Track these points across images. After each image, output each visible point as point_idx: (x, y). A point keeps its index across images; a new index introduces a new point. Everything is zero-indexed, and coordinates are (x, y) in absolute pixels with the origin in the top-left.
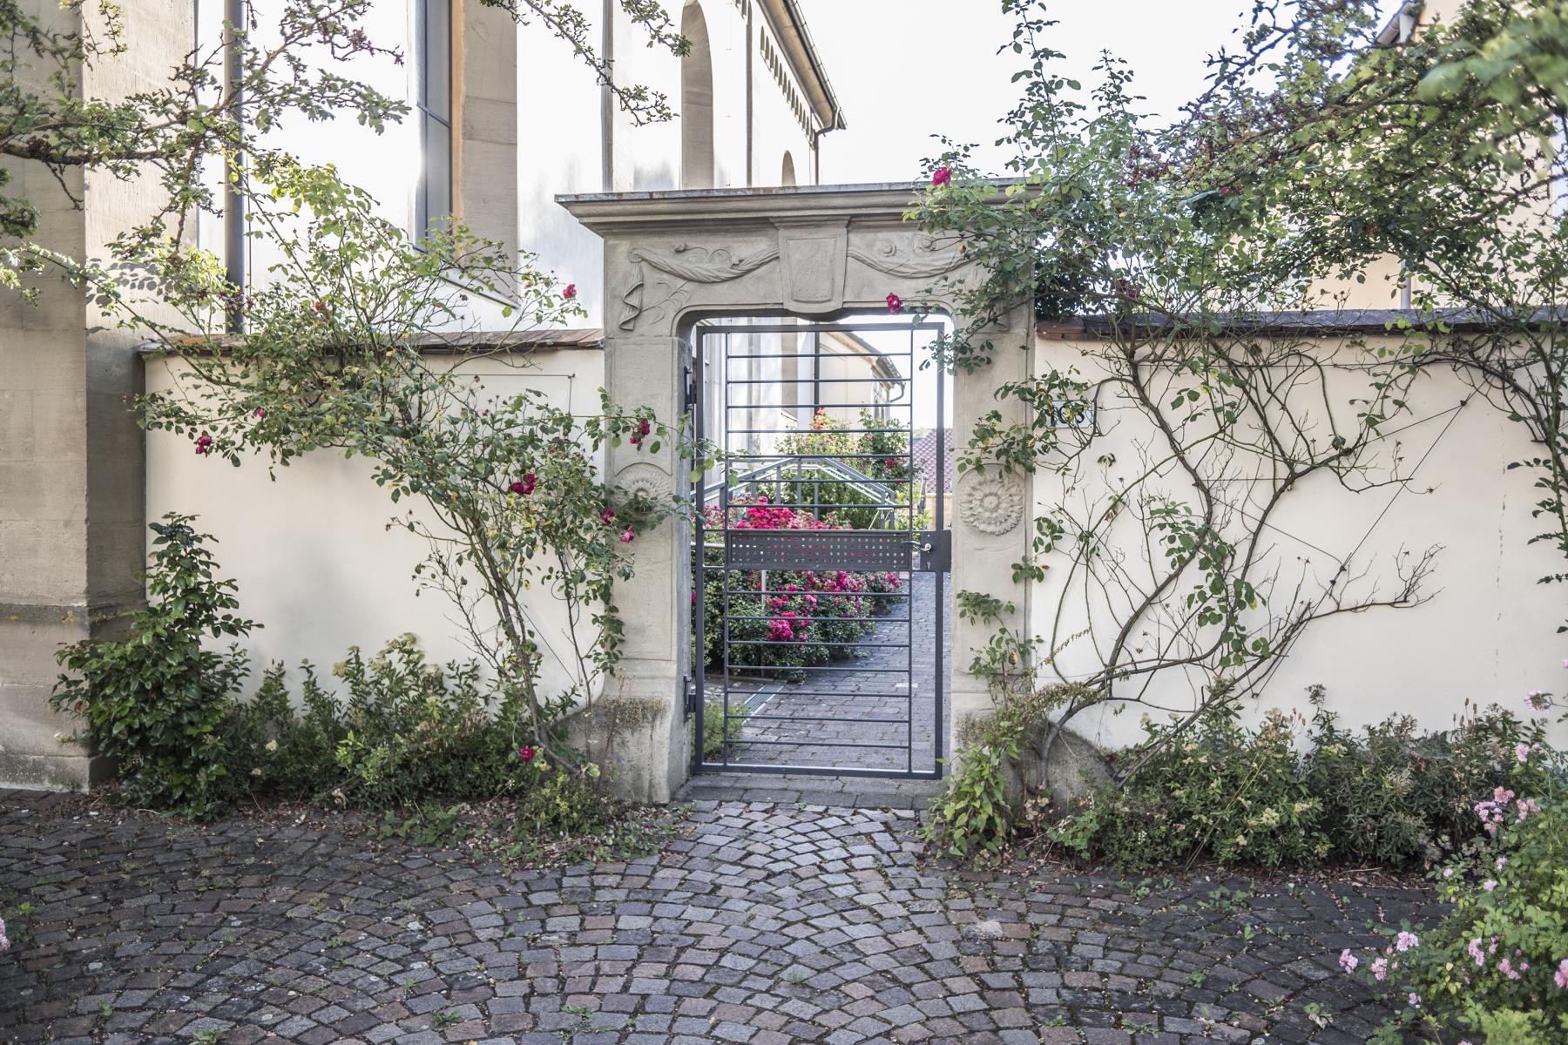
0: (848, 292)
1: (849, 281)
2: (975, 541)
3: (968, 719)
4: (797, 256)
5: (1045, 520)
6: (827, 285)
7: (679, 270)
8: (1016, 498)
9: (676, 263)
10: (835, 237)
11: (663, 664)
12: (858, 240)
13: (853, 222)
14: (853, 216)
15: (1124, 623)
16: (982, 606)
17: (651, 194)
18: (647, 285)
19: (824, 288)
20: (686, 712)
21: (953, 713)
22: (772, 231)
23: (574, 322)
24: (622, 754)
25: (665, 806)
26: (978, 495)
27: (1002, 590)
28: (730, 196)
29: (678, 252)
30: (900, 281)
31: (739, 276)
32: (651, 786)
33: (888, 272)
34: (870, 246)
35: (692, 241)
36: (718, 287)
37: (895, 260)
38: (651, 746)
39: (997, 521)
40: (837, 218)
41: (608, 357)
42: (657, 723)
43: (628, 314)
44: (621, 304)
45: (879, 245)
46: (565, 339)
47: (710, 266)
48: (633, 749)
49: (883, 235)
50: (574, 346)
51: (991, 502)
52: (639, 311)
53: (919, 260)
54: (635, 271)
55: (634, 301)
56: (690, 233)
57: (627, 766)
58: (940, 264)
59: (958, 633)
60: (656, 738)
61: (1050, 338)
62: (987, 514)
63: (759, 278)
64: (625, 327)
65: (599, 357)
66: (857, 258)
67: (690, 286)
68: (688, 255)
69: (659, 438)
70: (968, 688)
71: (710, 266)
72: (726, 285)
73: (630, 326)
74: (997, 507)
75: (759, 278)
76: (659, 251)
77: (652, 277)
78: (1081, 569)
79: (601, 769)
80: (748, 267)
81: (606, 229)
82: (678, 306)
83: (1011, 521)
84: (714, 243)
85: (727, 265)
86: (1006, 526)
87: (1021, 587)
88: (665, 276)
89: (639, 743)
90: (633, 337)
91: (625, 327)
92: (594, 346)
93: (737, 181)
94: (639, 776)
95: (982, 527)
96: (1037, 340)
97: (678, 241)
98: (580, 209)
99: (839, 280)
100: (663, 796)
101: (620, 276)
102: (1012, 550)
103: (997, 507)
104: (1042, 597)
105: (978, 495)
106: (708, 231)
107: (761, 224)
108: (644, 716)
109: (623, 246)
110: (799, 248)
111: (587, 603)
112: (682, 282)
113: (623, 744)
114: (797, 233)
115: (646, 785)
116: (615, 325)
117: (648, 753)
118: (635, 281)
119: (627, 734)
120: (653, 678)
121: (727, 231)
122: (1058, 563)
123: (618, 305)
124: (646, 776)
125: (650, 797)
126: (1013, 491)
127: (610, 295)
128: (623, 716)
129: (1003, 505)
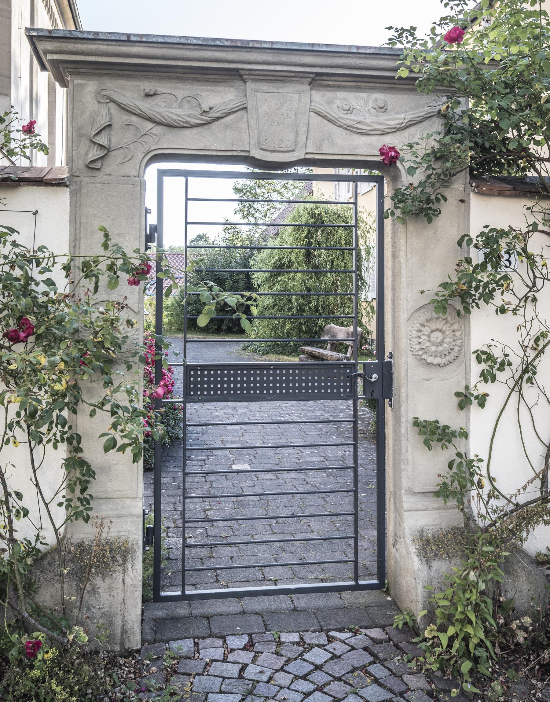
0: (310, 144)
1: (311, 134)
2: (421, 372)
3: (421, 536)
4: (264, 108)
5: (484, 353)
6: (291, 136)
7: (149, 112)
8: (458, 334)
9: (145, 106)
10: (299, 92)
11: (128, 502)
12: (320, 98)
13: (318, 80)
14: (318, 74)
16: (435, 434)
17: (129, 36)
18: (116, 126)
19: (288, 140)
21: (407, 531)
23: (40, 160)
24: (93, 602)
25: (138, 651)
26: (426, 330)
27: (448, 417)
29: (147, 95)
30: (356, 137)
32: (124, 631)
33: (347, 128)
34: (330, 102)
35: (161, 87)
36: (187, 132)
37: (352, 117)
38: (124, 591)
39: (443, 354)
41: (73, 195)
42: (129, 565)
43: (95, 153)
44: (88, 142)
45: (338, 102)
47: (179, 111)
48: (104, 595)
49: (341, 94)
50: (39, 182)
51: (437, 336)
52: (107, 150)
53: (374, 119)
54: (104, 112)
55: (103, 140)
56: (159, 78)
57: (98, 615)
58: (393, 123)
59: (410, 456)
60: (128, 581)
61: (481, 193)
62: (434, 348)
63: (227, 126)
64: (92, 167)
65: (63, 197)
66: (318, 114)
67: (158, 130)
69: (160, 275)
70: (419, 506)
71: (179, 111)
72: (194, 131)
73: (97, 165)
74: (442, 342)
75: (227, 126)
76: (128, 93)
77: (120, 118)
78: (515, 395)
79: (86, 632)
83: (454, 354)
84: (183, 90)
85: (197, 112)
87: (462, 413)
88: (134, 118)
89: (111, 589)
90: (100, 177)
91: (92, 167)
92: (59, 183)
94: (111, 623)
95: (429, 360)
96: (472, 195)
97: (149, 86)
99: (302, 133)
100: (135, 641)
101: (87, 115)
102: (451, 381)
103: (442, 342)
104: (479, 421)
105: (426, 330)
106: (177, 78)
107: (232, 75)
108: (114, 558)
109: (90, 86)
110: (266, 100)
111: (55, 447)
112: (150, 125)
113: (94, 591)
114: (264, 86)
115: (119, 631)
116: (80, 164)
117: (120, 598)
118: (103, 121)
119: (98, 581)
120: (119, 517)
121: (195, 80)
122: (497, 392)
123: (85, 144)
124: (118, 622)
125: (122, 644)
126: (456, 326)
127: (76, 134)
128: (88, 562)
129: (447, 340)
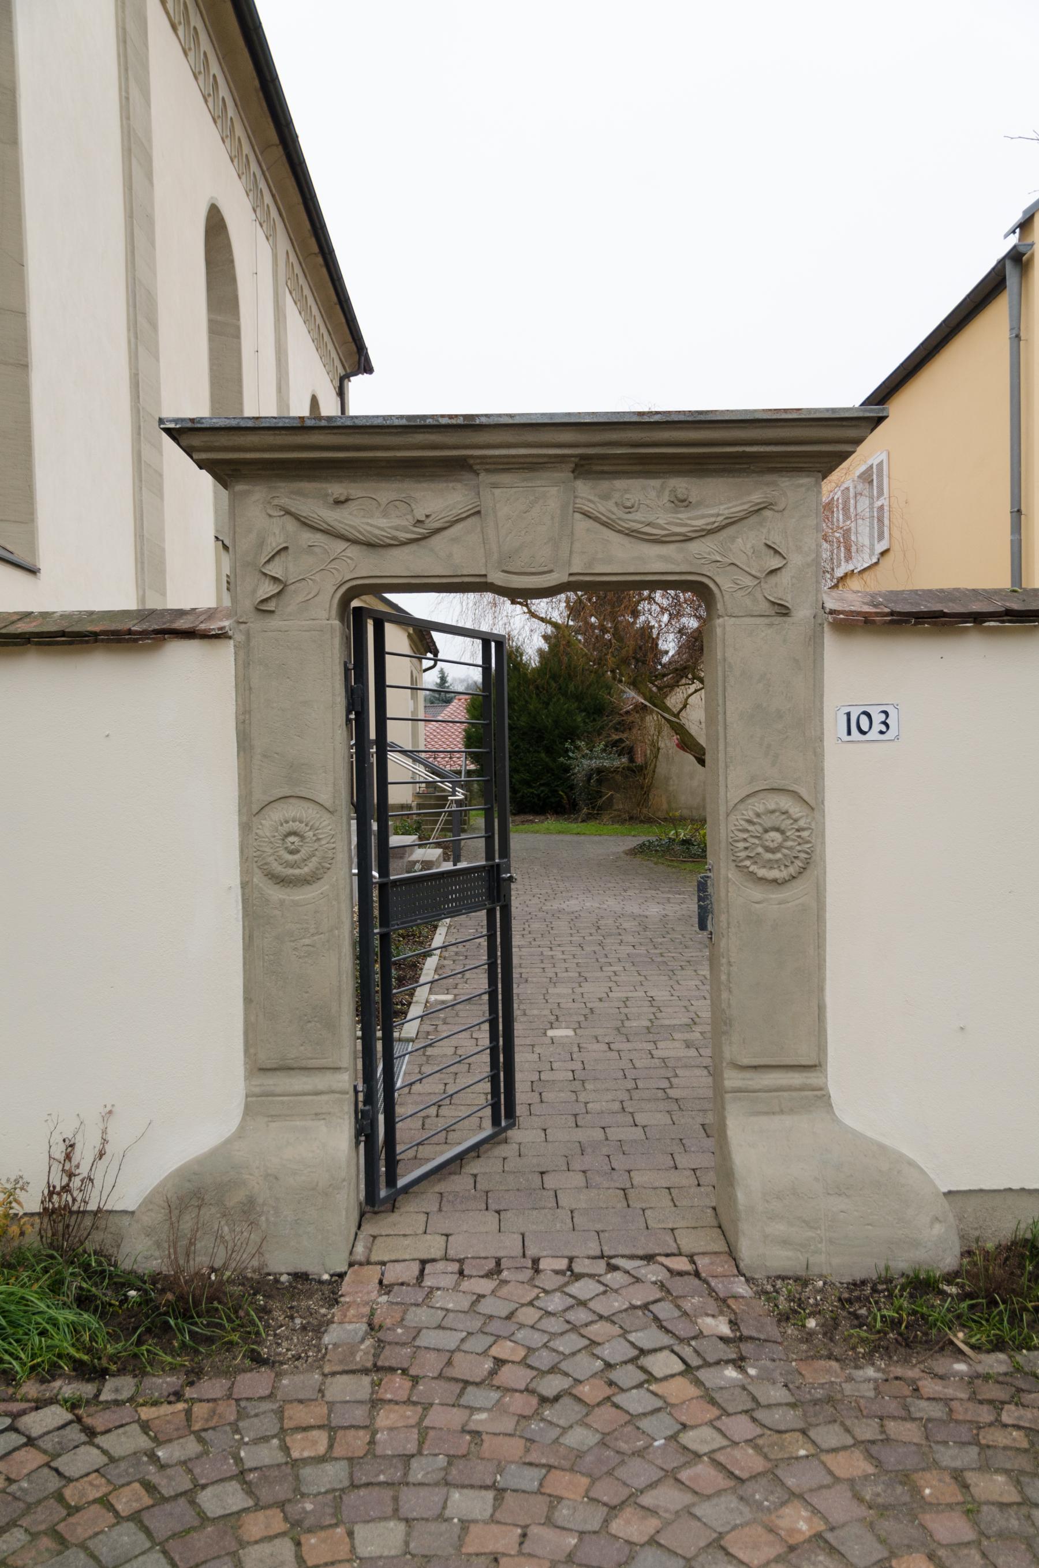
7: (340, 527)
9: (333, 517)
15: (351, 340)
20: (357, 1135)
22: (468, 476)
28: (258, 427)
31: (425, 538)
33: (631, 534)
36: (395, 552)
40: (562, 459)
43: (268, 589)
46: (182, 624)
47: (383, 522)
50: (189, 634)
58: (700, 523)
63: (455, 540)
65: (225, 655)
67: (353, 551)
68: (352, 506)
71: (383, 522)
73: (271, 606)
80: (437, 525)
81: (226, 471)
82: (339, 579)
84: (386, 492)
85: (407, 522)
86: (792, 870)
88: (319, 536)
93: (725, 1076)
98: (196, 441)
112: (344, 545)
116: (247, 604)
